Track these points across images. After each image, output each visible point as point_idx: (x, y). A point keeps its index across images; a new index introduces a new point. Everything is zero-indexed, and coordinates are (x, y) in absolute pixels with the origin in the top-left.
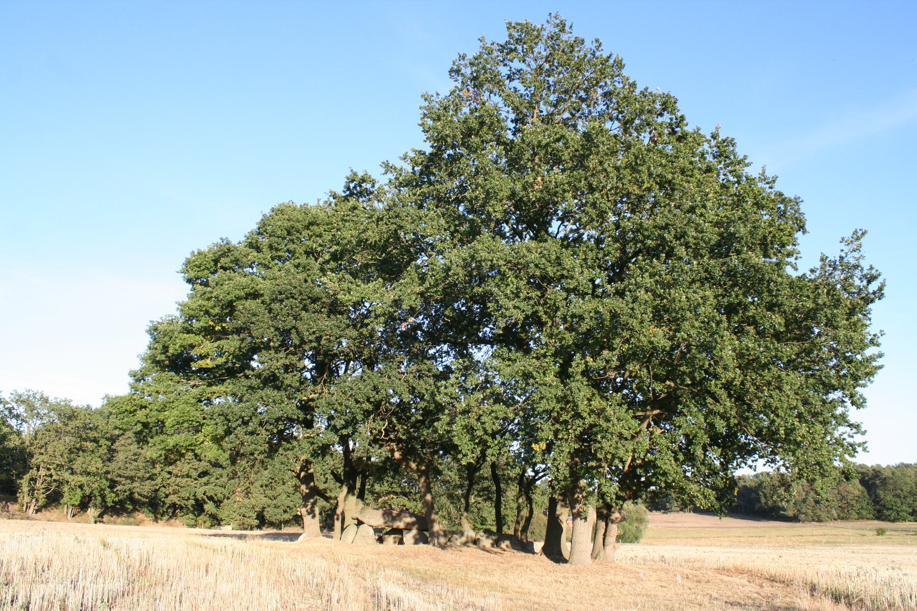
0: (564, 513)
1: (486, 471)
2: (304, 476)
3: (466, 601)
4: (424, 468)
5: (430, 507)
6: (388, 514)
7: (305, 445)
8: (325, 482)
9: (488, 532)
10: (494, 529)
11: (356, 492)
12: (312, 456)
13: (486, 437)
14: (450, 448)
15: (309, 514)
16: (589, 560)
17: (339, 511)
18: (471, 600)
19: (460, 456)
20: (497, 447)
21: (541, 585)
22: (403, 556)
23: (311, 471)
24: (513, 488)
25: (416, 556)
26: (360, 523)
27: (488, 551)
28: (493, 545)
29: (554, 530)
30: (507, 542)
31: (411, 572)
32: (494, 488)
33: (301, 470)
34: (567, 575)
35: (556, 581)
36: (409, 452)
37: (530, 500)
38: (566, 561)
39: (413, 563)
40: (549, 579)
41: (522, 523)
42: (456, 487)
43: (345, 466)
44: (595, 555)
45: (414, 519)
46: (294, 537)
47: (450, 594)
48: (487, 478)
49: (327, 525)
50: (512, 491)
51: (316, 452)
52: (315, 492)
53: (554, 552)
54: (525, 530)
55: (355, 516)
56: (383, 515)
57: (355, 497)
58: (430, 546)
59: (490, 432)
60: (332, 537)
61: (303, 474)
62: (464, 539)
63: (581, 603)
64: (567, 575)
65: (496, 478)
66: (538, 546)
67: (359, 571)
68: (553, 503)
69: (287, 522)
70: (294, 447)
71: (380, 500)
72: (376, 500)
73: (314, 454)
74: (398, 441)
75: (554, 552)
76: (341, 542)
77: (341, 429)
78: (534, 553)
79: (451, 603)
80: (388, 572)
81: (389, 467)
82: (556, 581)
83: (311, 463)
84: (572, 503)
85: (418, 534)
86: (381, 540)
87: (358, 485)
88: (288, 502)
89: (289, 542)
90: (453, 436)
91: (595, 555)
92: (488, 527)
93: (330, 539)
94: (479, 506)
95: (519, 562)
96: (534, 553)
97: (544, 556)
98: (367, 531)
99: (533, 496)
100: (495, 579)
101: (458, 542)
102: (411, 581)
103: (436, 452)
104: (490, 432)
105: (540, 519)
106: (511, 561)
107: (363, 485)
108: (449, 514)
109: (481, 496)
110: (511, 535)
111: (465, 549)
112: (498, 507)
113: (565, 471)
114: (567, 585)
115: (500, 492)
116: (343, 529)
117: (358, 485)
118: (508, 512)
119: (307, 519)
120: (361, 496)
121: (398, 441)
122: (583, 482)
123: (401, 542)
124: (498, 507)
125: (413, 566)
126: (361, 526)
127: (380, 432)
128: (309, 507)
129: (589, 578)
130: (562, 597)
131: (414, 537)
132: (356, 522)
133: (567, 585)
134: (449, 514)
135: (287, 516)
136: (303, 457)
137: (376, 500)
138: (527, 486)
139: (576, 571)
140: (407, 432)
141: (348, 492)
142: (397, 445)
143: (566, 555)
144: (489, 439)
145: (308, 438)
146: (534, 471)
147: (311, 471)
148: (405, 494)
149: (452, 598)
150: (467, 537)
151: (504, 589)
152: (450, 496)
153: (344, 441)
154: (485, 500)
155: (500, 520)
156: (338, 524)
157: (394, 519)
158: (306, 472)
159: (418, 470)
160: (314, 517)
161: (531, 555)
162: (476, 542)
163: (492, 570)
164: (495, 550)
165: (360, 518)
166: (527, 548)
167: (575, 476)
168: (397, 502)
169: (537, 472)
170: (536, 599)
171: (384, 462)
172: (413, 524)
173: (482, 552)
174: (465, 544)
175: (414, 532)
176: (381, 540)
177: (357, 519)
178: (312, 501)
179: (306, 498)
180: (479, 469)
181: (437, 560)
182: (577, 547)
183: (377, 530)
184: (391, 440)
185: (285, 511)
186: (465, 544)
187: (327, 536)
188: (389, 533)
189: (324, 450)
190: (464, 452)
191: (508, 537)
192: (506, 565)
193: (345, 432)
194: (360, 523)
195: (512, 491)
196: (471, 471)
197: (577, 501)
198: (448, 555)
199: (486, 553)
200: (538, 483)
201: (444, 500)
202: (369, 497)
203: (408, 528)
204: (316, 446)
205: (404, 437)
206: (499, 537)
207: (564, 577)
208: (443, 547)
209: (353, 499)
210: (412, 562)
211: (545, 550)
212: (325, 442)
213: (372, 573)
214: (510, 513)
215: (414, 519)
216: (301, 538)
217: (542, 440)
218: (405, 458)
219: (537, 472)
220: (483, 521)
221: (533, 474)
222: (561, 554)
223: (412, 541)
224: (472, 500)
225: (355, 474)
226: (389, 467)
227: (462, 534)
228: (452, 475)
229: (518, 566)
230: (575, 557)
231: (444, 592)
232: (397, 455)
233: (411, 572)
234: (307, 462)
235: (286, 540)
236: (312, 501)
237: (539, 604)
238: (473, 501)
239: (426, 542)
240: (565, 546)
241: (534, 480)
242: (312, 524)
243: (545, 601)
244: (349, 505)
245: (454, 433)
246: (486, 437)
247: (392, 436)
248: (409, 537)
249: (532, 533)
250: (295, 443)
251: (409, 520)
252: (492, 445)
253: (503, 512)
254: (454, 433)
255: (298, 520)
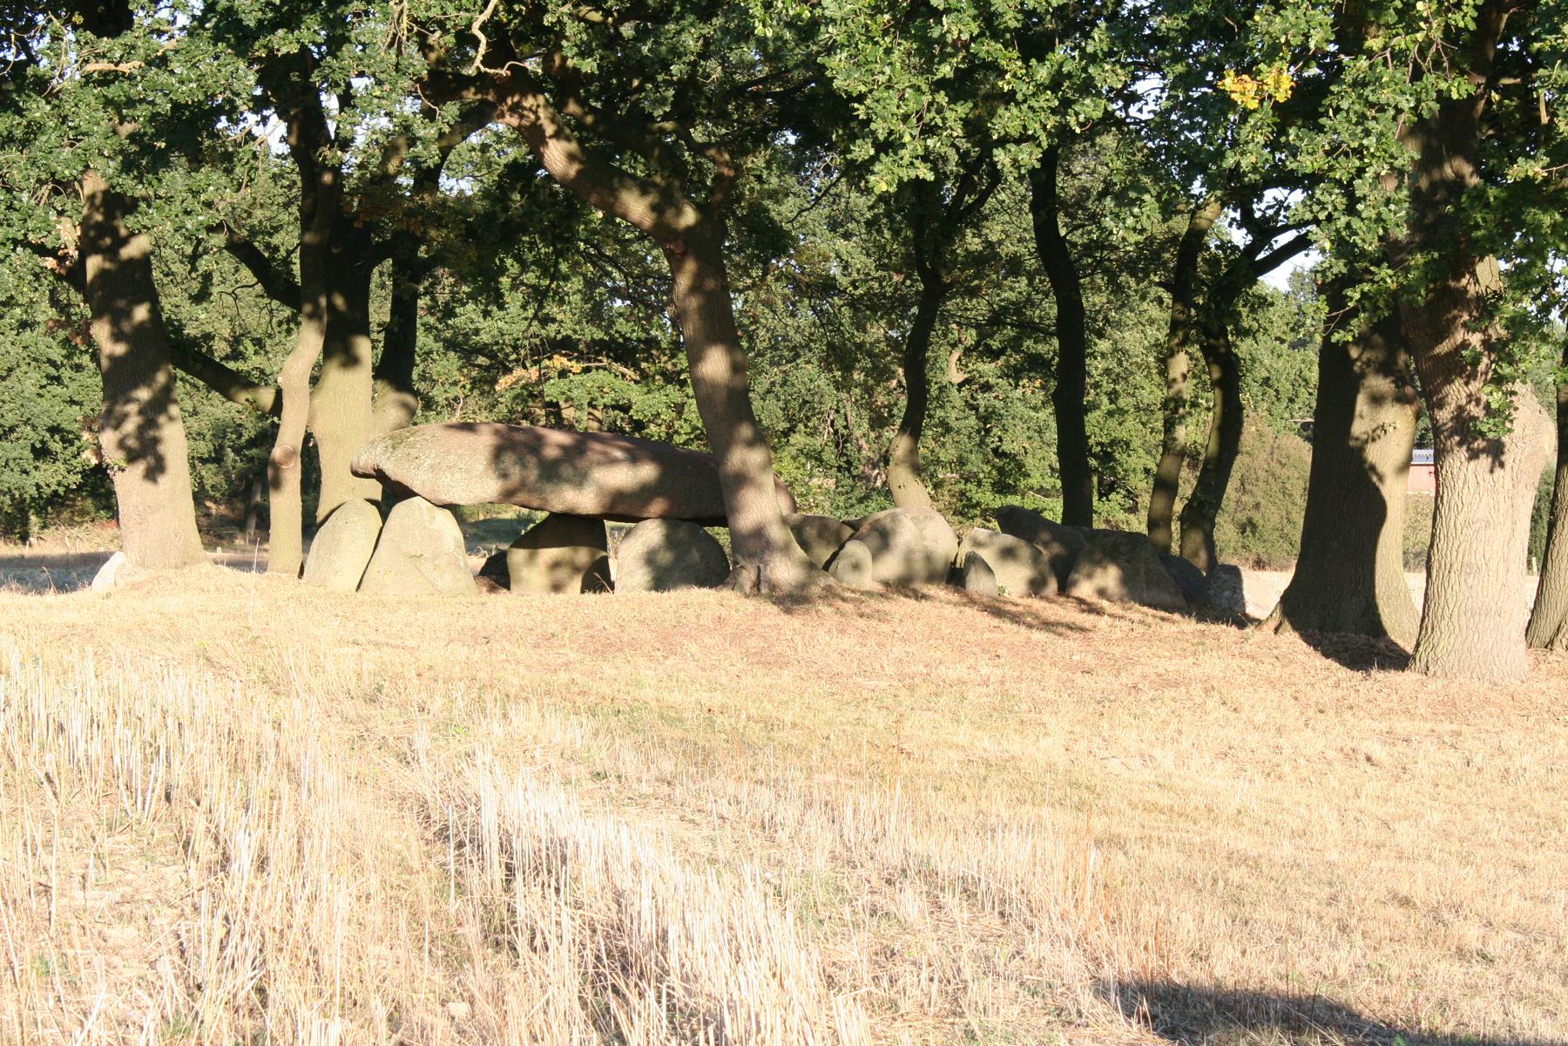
0: (1387, 431)
1: (1008, 227)
2: (102, 274)
3: (891, 854)
4: (689, 217)
5: (730, 409)
6: (514, 445)
7: (90, 114)
8: (201, 297)
9: (1018, 522)
10: (1054, 510)
11: (366, 349)
12: (128, 166)
13: (989, 49)
14: (822, 115)
15: (132, 457)
16: (1516, 653)
17: (289, 439)
18: (915, 846)
19: (862, 150)
20: (1049, 99)
21: (1272, 773)
22: (602, 646)
23: (132, 250)
24: (1154, 311)
25: (668, 641)
26: (394, 493)
27: (1015, 618)
28: (1036, 586)
29: (1343, 511)
30: (1110, 577)
31: (625, 717)
32: (1049, 309)
33: (87, 246)
34: (1402, 726)
35: (1350, 755)
36: (613, 136)
37: (1228, 375)
38: (1398, 660)
39: (647, 680)
40: (1311, 742)
41: (1187, 483)
42: (868, 306)
43: (306, 222)
44: (1545, 629)
45: (647, 472)
46: (75, 572)
47: (814, 818)
48: (1014, 266)
49: (237, 503)
50: (1136, 328)
51: (146, 149)
52: (167, 352)
53: (1339, 614)
54: (1202, 513)
55: (367, 461)
56: (498, 454)
57: (362, 377)
58: (726, 594)
59: (1011, 20)
60: (262, 567)
61: (94, 264)
62: (891, 566)
63: (1465, 860)
64: (1402, 726)
65: (1060, 265)
66: (1264, 589)
67: (384, 721)
68: (1337, 387)
69: (54, 505)
70: (34, 130)
71: (504, 382)
72: (484, 383)
73: (142, 158)
74: (564, 85)
75: (1339, 614)
76: (305, 587)
77: (266, 28)
78: (1242, 621)
79: (820, 862)
80: (524, 721)
81: (523, 223)
82: (1350, 755)
83: (128, 205)
84: (1422, 389)
85: (670, 541)
86: (497, 574)
87: (380, 311)
88: (51, 408)
89: (51, 597)
90: (830, 49)
91: (1545, 629)
92: (1030, 502)
93: (251, 577)
94: (983, 400)
95: (1171, 665)
96: (1242, 621)
97: (1291, 639)
98: (427, 530)
99: (1244, 348)
100: (1045, 747)
101: (868, 579)
102: (630, 763)
103: (760, 137)
104: (1011, 20)
105: (1277, 450)
106: (1132, 661)
107: (404, 309)
108: (841, 441)
109: (995, 355)
110: (1134, 537)
111: (902, 606)
112: (1070, 406)
113: (1386, 208)
114: (1403, 770)
115: (1075, 329)
116: (310, 527)
117: (380, 311)
118: (1130, 428)
119: (128, 482)
120: (395, 368)
121: (564, 85)
122: (1490, 272)
123: (597, 578)
124: (1070, 406)
125: (648, 694)
126: (400, 510)
127: (465, 38)
128: (130, 426)
129: (1511, 740)
130: (1370, 832)
131: (650, 559)
132: (375, 489)
133: (1403, 770)
134: (841, 441)
135: (50, 476)
136: (93, 184)
137: (484, 383)
138: (1211, 299)
139: (1448, 707)
140: (604, 37)
141: (328, 352)
142: (558, 105)
143: (1400, 626)
144: (1010, 60)
145: (106, 79)
146: (1247, 221)
147: (135, 248)
148: (623, 352)
149: (826, 840)
150: (908, 559)
151: (1081, 795)
152: (840, 357)
153: (291, 89)
154: (1014, 374)
155: (1081, 466)
156: (285, 505)
157: (551, 472)
158: (111, 253)
159: (661, 233)
160: (155, 471)
161: (1229, 632)
162: (954, 576)
163: (1036, 707)
164: (1062, 599)
165: (394, 472)
166: (1206, 595)
167: (1446, 234)
168: (587, 389)
169: (1263, 230)
170: (1245, 843)
171: (497, 195)
172: (645, 493)
173: (985, 620)
174: (903, 585)
175: (650, 533)
176: (497, 574)
177: (380, 475)
178: (144, 394)
179: (119, 380)
180: (973, 216)
181: (769, 660)
182: (1457, 594)
183: (476, 530)
184: (524, 83)
185: (41, 453)
186: (903, 585)
187: (244, 565)
188: (535, 538)
189: (188, 133)
190: (880, 128)
191: (1117, 547)
192: (1104, 681)
193: (284, 43)
194: (394, 493)
195: (1136, 328)
196: (928, 224)
197: (1458, 366)
198: (820, 635)
199: (1007, 625)
200: (1275, 281)
201: (810, 374)
202: (441, 369)
203: (625, 508)
204: (142, 111)
205: (589, 66)
206: (1065, 549)
207: (1389, 738)
208: (793, 600)
209: (354, 386)
210: (648, 674)
211: (1294, 608)
212: (188, 93)
213: (443, 727)
214: (1127, 428)
215: (647, 472)
216: (106, 572)
217: (1272, 53)
218: (598, 174)
219: (1263, 230)
220: (1008, 472)
221: (1240, 238)
222: (1376, 628)
223: (642, 576)
224: (950, 369)
225: (358, 258)
226: (523, 223)
227: (882, 538)
228: (846, 257)
229: (1165, 682)
230: (1446, 640)
231: (788, 812)
232: (557, 156)
233: (625, 717)
234: (115, 204)
235: (39, 588)
236: (144, 394)
237: (1254, 865)
238: (957, 377)
239: (714, 571)
240: (1398, 591)
241: (1248, 266)
242: (157, 506)
243: (1287, 849)
244: (336, 409)
245: (830, 32)
246: (989, 49)
247: (532, 65)
248: (633, 549)
249: (1248, 527)
250: (38, 109)
251: (624, 475)
252: (1023, 89)
253: (1096, 426)
254: (830, 32)
255: (97, 490)
